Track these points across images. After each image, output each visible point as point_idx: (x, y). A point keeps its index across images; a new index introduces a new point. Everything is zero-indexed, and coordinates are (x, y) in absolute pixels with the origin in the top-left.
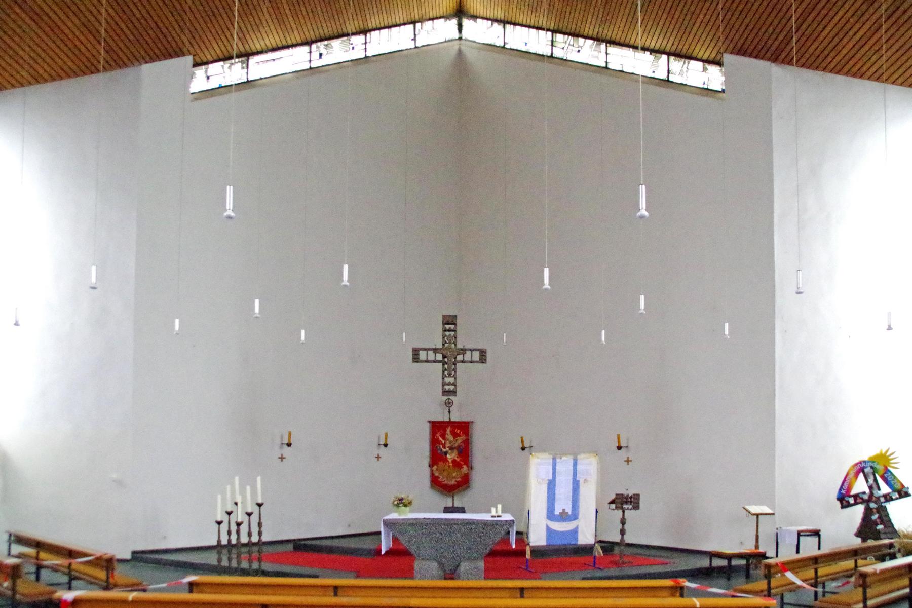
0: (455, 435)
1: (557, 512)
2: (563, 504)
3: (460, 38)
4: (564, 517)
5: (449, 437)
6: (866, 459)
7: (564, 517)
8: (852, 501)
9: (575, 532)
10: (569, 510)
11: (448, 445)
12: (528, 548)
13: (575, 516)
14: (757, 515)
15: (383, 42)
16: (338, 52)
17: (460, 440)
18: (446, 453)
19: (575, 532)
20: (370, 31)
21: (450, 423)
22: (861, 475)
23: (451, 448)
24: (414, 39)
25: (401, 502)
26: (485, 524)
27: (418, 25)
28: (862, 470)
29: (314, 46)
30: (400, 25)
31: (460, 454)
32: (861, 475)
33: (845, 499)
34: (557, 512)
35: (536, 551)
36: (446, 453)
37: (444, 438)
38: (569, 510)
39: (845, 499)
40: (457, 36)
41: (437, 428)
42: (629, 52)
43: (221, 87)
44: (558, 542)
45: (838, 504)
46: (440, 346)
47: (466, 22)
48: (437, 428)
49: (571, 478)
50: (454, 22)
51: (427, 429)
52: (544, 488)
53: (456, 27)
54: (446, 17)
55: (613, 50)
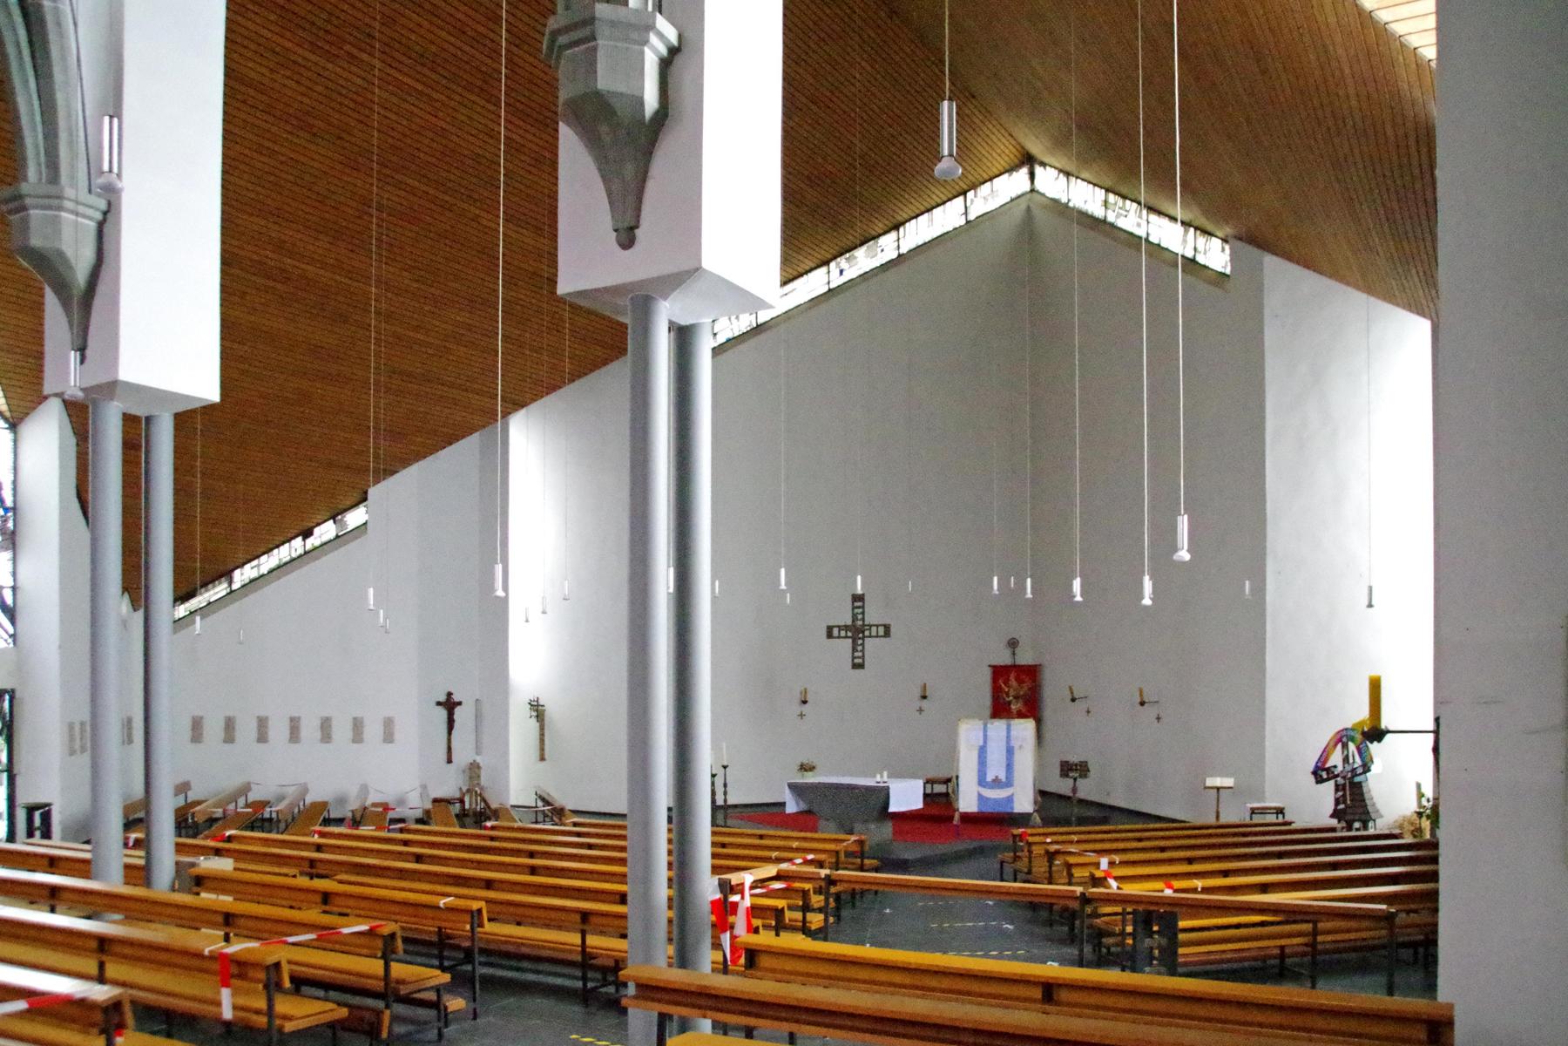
0: (1020, 681)
1: (989, 778)
2: (996, 770)
3: (1032, 190)
4: (997, 783)
5: (1013, 683)
6: (1349, 725)
7: (997, 783)
8: (1324, 775)
9: (1010, 799)
10: (1003, 777)
11: (1012, 693)
12: (957, 816)
13: (1009, 783)
14: (1218, 789)
15: (918, 232)
16: (864, 260)
17: (1025, 687)
18: (1010, 703)
19: (1010, 799)
20: (903, 224)
21: (1014, 667)
22: (1339, 746)
23: (1016, 698)
24: (966, 213)
25: (805, 768)
26: (868, 789)
27: (970, 194)
28: (1340, 740)
29: (833, 265)
30: (944, 203)
31: (1026, 703)
32: (1339, 746)
33: (1321, 773)
34: (989, 778)
35: (967, 818)
36: (1010, 703)
37: (1006, 683)
38: (1003, 777)
39: (1321, 773)
40: (1027, 187)
41: (999, 672)
42: (1165, 221)
43: (728, 340)
44: (988, 809)
45: (1312, 778)
46: (849, 622)
47: (1038, 170)
48: (999, 672)
49: (1004, 743)
50: (1024, 171)
51: (987, 676)
52: (975, 754)
53: (1027, 177)
54: (1011, 169)
55: (1153, 218)
